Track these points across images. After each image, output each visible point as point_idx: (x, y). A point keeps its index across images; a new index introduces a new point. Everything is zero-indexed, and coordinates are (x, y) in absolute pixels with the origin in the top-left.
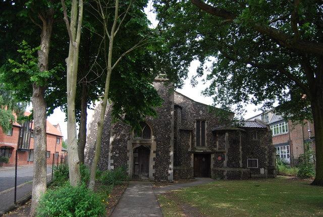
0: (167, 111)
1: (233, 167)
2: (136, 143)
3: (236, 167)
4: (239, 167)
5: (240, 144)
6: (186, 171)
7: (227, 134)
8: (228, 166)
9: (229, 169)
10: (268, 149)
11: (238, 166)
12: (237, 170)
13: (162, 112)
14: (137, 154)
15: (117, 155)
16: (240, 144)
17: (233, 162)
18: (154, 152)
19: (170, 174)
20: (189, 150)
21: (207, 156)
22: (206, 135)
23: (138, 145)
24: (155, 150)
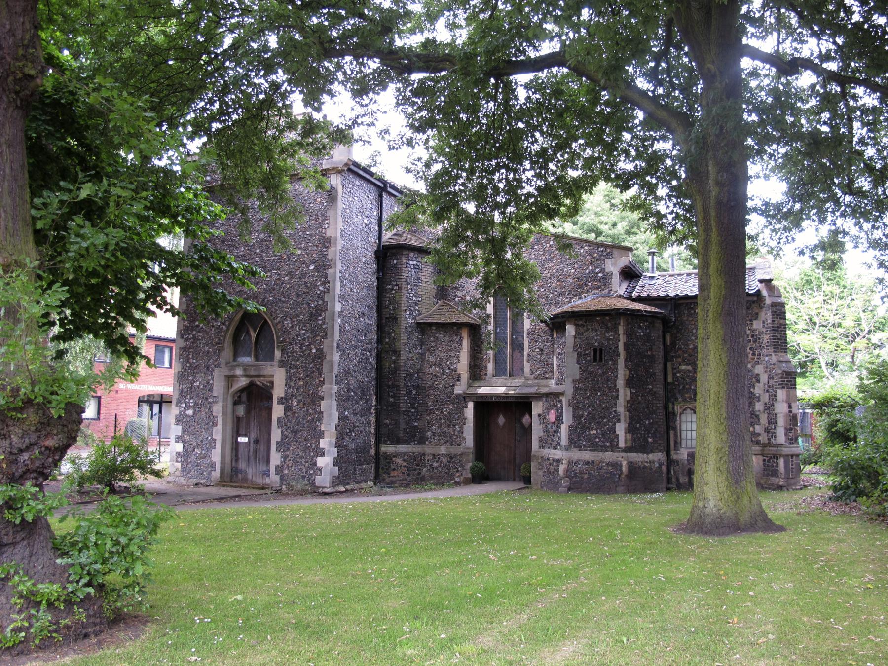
0: (317, 269)
1: (594, 447)
2: (234, 376)
3: (604, 449)
4: (614, 448)
5: (621, 361)
6: (444, 460)
7: (570, 329)
8: (574, 443)
9: (577, 455)
10: (764, 378)
11: (610, 442)
12: (608, 456)
13: (303, 275)
14: (241, 410)
15: (190, 412)
16: (621, 361)
17: (590, 427)
18: (280, 401)
19: (320, 469)
20: (458, 390)
21: (520, 406)
22: (525, 335)
23: (243, 382)
24: (283, 395)
